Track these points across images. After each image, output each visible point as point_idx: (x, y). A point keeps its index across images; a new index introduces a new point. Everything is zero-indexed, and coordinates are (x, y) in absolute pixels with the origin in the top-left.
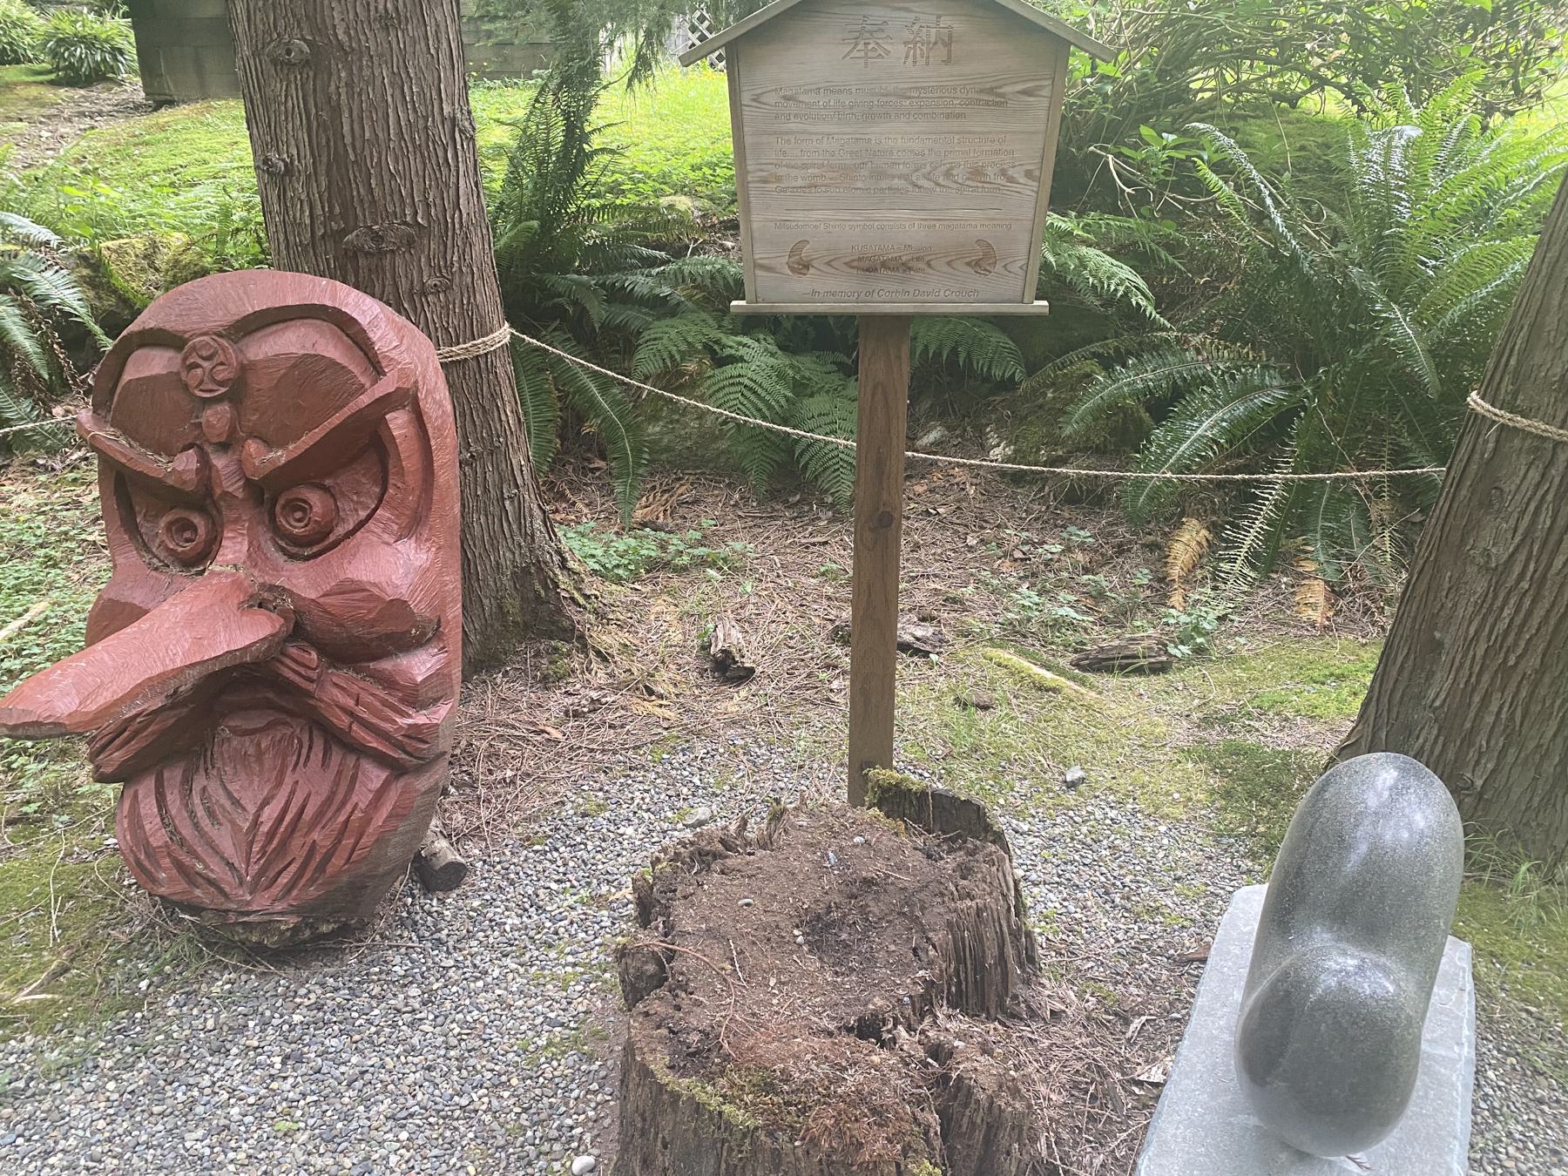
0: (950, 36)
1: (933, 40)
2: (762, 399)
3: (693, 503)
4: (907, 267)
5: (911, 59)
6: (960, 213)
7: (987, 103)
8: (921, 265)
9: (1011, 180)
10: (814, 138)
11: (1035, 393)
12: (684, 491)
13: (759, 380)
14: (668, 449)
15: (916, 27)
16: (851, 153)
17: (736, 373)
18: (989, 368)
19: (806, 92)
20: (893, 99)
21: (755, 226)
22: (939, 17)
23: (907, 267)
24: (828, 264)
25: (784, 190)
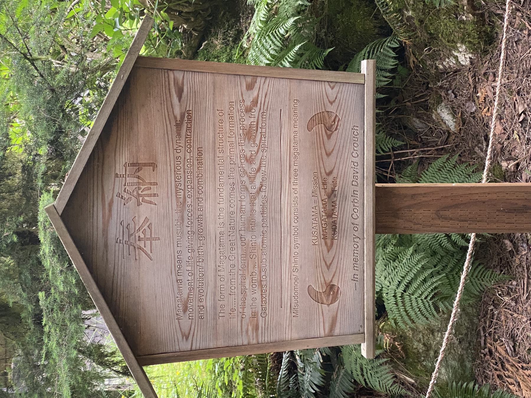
0: (133, 165)
1: (136, 180)
2: (416, 276)
3: (514, 341)
4: (332, 194)
5: (152, 199)
6: (284, 147)
7: (189, 129)
8: (330, 180)
9: (255, 102)
10: (219, 283)
11: (410, 28)
12: (503, 348)
13: (398, 278)
14: (461, 360)
15: (126, 196)
16: (232, 249)
17: (393, 300)
18: (385, 70)
19: (180, 292)
20: (186, 213)
21: (295, 336)
22: (117, 175)
23: (332, 194)
24: (328, 267)
25: (264, 310)
